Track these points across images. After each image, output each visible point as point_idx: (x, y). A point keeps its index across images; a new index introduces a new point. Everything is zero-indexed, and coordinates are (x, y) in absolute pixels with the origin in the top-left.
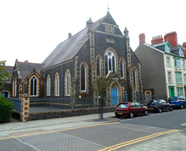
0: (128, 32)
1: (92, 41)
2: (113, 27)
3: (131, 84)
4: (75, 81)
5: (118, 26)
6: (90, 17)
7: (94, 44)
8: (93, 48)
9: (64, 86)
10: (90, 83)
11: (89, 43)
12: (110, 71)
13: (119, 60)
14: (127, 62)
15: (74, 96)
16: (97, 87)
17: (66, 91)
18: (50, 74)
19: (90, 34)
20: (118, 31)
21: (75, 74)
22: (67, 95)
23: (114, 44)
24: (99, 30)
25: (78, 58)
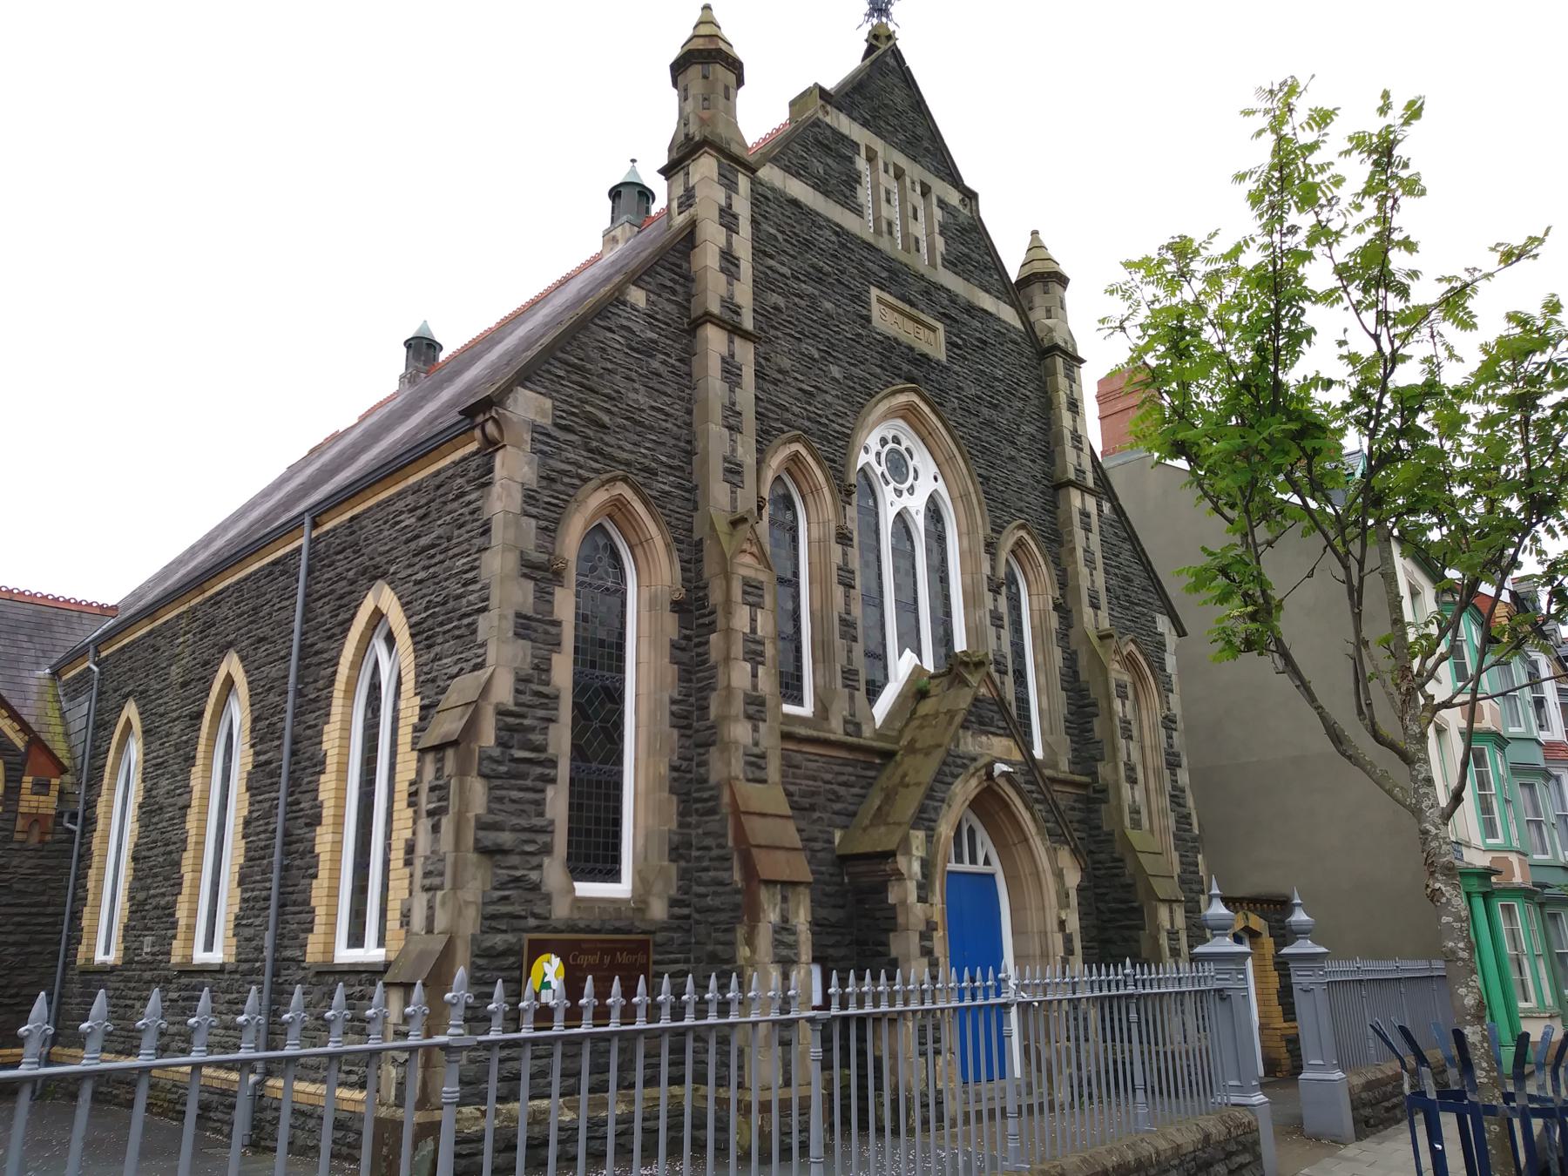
0: (1063, 281)
1: (729, 259)
2: (926, 191)
4: (488, 736)
5: (970, 196)
6: (1035, 233)
7: (744, 294)
8: (735, 330)
9: (316, 820)
10: (689, 787)
11: (688, 279)
12: (909, 657)
13: (991, 547)
14: (1064, 581)
15: (463, 954)
16: (791, 827)
17: (334, 893)
18: (142, 696)
19: (705, 167)
20: (969, 240)
21: (493, 628)
24: (797, 175)
25: (547, 422)
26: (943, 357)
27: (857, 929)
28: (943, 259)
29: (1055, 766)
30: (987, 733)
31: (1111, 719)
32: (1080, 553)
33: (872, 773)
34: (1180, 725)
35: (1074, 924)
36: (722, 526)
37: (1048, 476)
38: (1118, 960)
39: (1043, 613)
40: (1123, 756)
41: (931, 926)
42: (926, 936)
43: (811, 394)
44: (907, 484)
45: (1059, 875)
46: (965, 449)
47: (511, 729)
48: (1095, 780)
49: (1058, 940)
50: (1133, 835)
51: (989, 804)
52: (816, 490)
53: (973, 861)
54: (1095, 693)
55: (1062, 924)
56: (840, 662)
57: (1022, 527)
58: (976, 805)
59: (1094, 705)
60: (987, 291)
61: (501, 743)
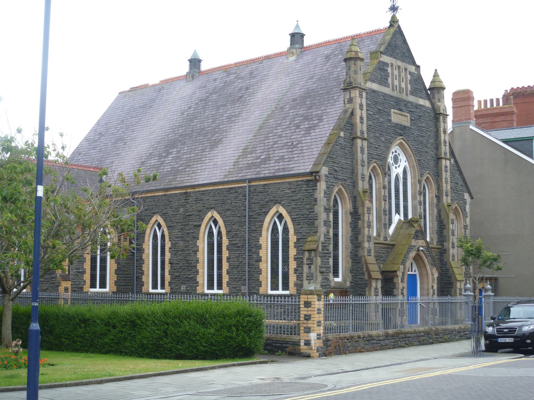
0: (444, 89)
2: (406, 69)
3: (451, 259)
5: (418, 67)
6: (436, 70)
10: (356, 258)
13: (420, 182)
22: (151, 291)
23: (410, 129)
26: (409, 125)
27: (388, 288)
28: (410, 92)
29: (432, 244)
30: (418, 239)
31: (449, 230)
32: (444, 180)
33: (389, 250)
34: (469, 228)
35: (435, 287)
36: (361, 193)
37: (436, 155)
38: (447, 295)
39: (432, 199)
40: (451, 241)
41: (404, 288)
42: (402, 290)
43: (377, 148)
44: (398, 165)
45: (433, 275)
46: (414, 152)
47: (324, 246)
48: (443, 247)
49: (431, 291)
50: (452, 263)
51: (418, 259)
52: (378, 174)
53: (412, 271)
54: (445, 222)
55: (433, 287)
56: (383, 221)
57: (429, 173)
58: (415, 259)
59: (445, 226)
60: (421, 98)
61: (323, 250)
